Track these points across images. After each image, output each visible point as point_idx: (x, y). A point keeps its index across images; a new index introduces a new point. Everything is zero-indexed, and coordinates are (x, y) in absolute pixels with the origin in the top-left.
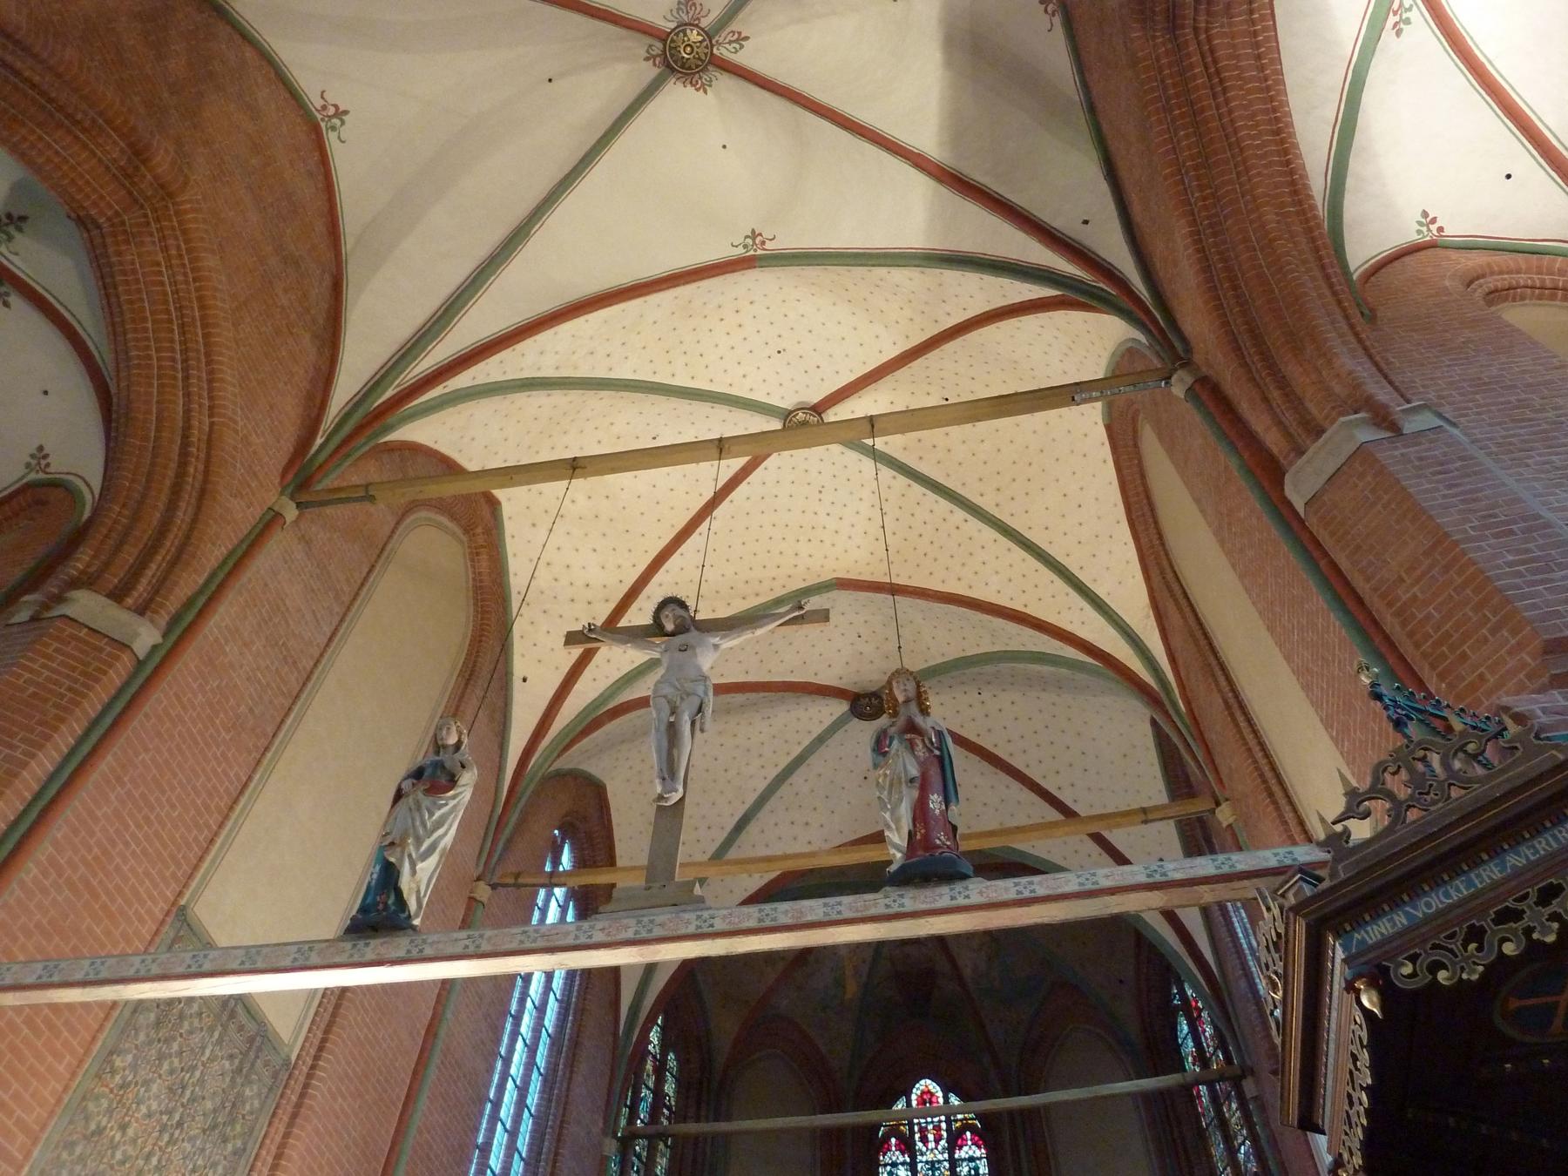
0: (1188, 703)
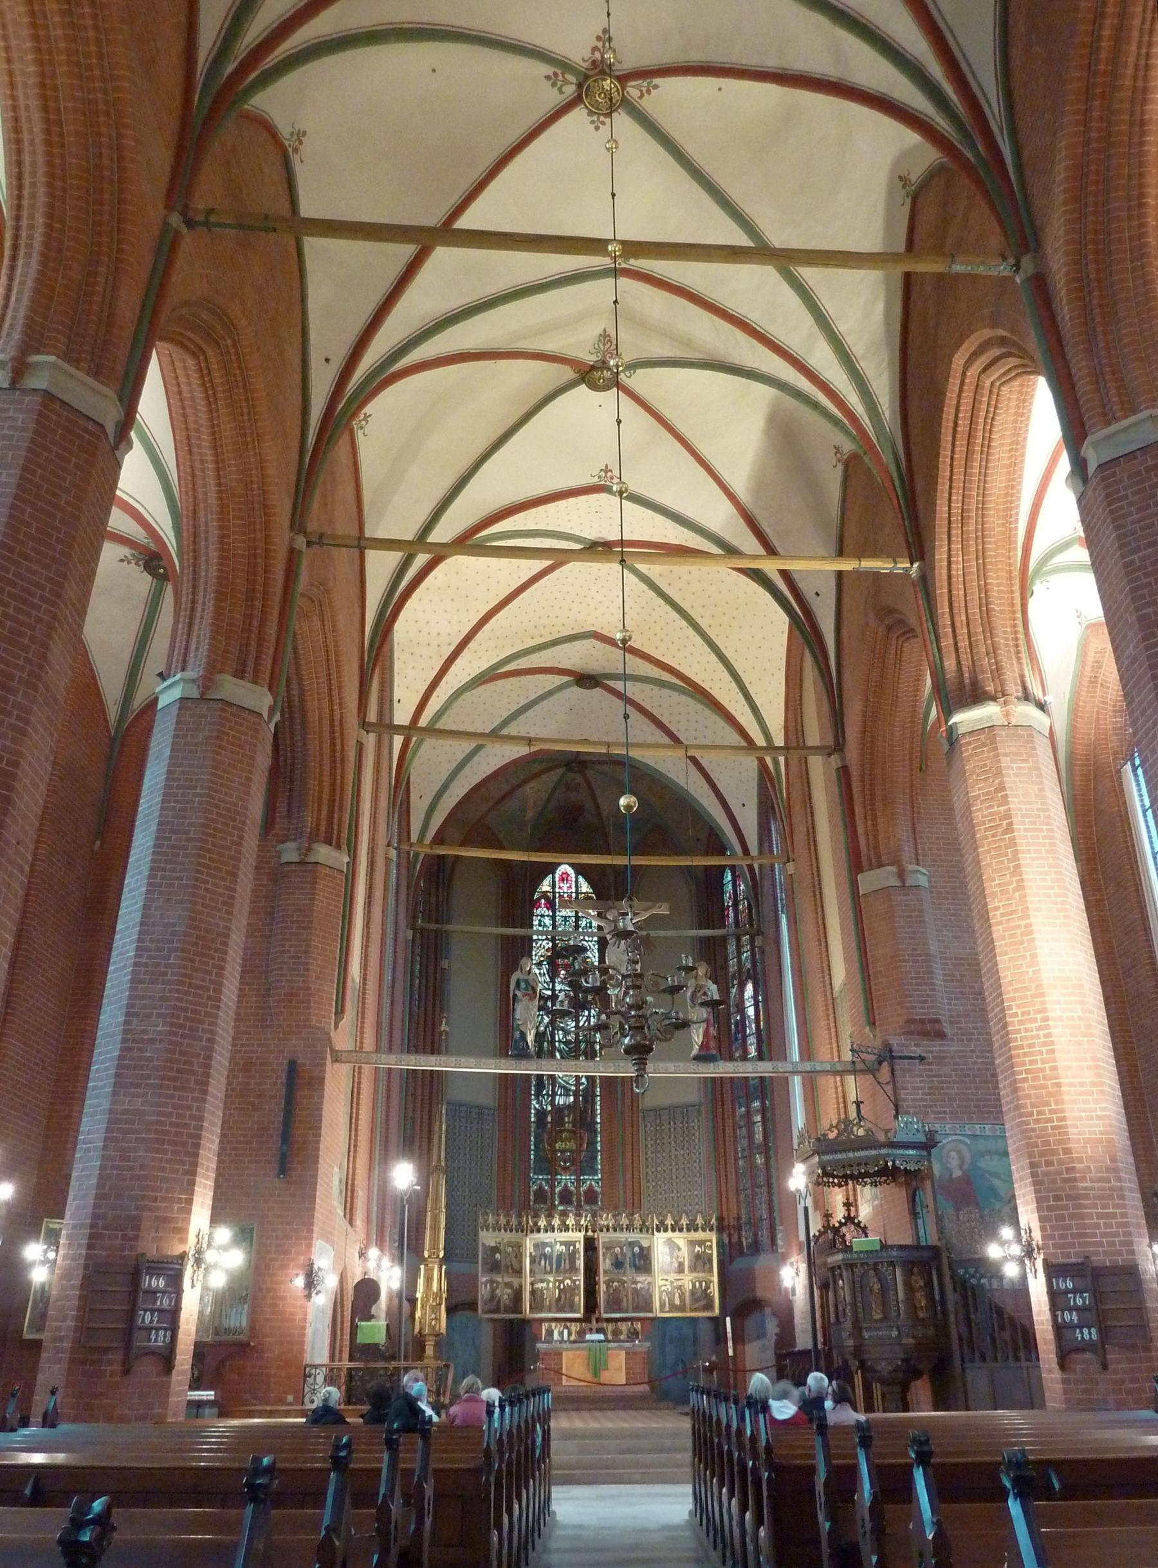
0: (788, 794)
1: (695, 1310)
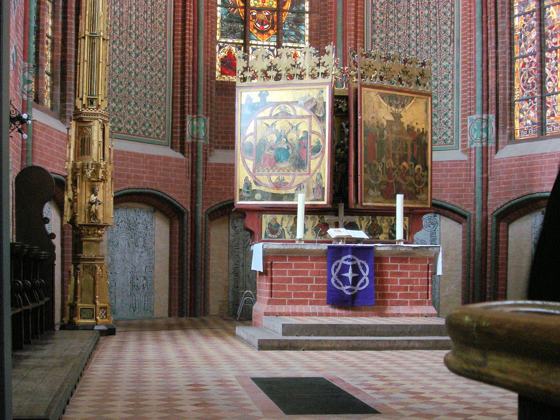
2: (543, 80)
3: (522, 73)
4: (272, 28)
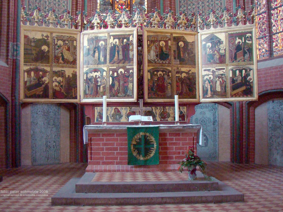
1: (236, 95)
2: (270, 26)
3: (259, 23)
4: (127, 7)
